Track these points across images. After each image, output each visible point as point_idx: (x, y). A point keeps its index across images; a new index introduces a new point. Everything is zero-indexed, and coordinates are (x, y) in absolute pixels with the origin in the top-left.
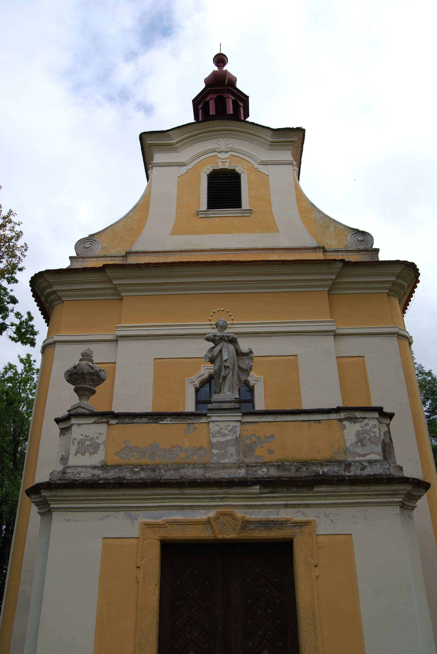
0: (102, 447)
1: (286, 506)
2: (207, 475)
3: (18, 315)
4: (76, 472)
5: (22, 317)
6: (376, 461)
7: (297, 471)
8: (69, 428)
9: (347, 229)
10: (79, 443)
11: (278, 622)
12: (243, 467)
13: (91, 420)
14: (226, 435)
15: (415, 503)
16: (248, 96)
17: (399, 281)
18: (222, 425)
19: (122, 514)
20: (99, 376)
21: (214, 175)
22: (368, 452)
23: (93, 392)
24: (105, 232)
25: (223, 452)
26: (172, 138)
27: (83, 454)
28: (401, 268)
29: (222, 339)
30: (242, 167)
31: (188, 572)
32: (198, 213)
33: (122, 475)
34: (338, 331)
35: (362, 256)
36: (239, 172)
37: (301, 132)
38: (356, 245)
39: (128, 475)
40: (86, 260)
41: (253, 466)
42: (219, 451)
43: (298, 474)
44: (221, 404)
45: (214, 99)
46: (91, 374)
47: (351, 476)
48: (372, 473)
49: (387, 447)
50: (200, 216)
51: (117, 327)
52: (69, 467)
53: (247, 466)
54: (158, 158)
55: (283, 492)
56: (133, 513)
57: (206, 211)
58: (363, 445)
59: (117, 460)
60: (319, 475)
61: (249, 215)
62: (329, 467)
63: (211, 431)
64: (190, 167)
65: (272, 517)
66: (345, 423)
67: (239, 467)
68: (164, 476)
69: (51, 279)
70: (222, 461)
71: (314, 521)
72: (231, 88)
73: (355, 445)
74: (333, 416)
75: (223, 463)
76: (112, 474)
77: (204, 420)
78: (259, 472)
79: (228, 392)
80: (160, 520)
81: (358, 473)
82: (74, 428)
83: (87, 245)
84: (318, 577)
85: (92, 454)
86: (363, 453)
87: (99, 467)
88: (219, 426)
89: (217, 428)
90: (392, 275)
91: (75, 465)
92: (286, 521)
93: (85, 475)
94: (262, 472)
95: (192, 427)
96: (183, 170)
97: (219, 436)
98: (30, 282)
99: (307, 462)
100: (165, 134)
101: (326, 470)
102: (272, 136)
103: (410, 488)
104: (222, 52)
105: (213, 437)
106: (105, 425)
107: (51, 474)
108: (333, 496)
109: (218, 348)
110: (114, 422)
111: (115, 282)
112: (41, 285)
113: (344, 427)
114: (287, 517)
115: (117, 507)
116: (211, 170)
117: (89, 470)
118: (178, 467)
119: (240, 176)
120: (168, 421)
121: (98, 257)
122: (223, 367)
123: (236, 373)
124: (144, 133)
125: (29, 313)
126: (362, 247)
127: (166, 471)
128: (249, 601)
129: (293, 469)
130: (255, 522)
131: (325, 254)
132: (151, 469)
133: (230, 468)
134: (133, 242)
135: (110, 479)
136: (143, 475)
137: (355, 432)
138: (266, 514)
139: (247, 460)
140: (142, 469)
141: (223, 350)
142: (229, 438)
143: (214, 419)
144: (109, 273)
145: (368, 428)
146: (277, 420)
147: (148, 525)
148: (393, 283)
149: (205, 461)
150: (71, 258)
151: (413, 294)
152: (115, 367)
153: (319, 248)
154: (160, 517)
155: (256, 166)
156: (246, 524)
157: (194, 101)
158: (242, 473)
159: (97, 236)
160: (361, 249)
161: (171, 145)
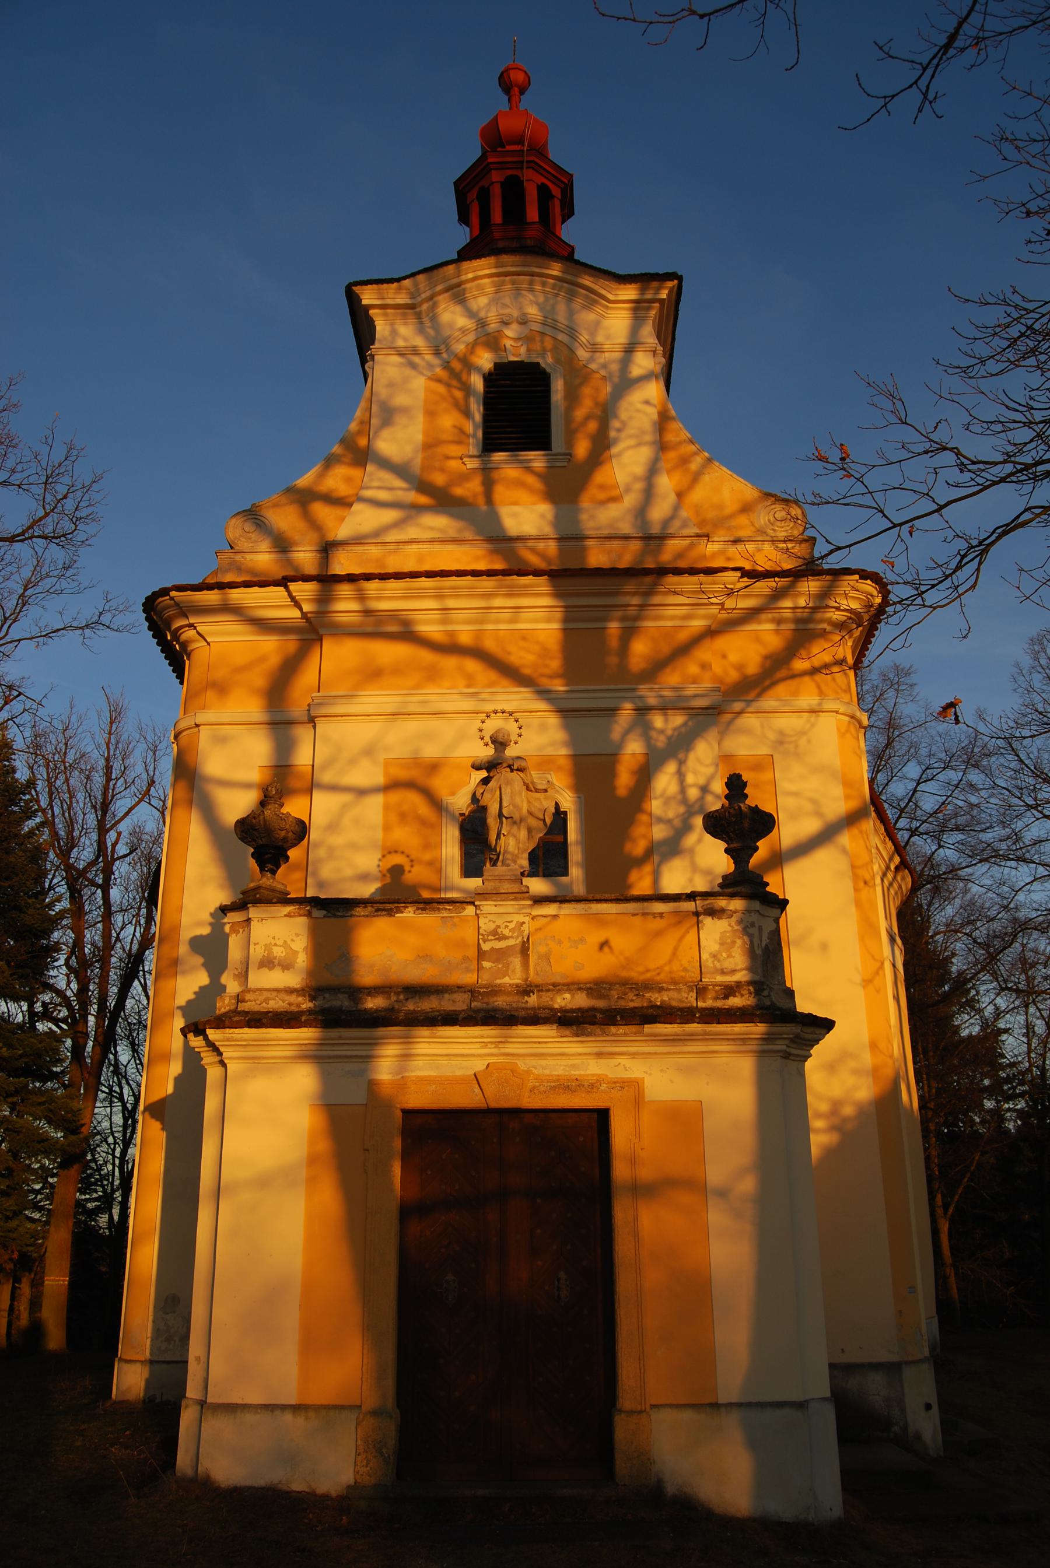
14: (505, 938)
15: (809, 1050)
25: (500, 966)
36: (548, 370)
42: (494, 965)
45: (499, 184)
52: (249, 991)
55: (595, 1035)
63: (481, 931)
65: (577, 1073)
87: (299, 991)
88: (494, 922)
91: (259, 986)
93: (277, 1004)
94: (563, 1001)
97: (495, 939)
98: (143, 605)
112: (166, 611)
117: (283, 995)
119: (549, 378)
137: (719, 935)
138: (568, 1069)
151: (878, 625)
157: (456, 184)
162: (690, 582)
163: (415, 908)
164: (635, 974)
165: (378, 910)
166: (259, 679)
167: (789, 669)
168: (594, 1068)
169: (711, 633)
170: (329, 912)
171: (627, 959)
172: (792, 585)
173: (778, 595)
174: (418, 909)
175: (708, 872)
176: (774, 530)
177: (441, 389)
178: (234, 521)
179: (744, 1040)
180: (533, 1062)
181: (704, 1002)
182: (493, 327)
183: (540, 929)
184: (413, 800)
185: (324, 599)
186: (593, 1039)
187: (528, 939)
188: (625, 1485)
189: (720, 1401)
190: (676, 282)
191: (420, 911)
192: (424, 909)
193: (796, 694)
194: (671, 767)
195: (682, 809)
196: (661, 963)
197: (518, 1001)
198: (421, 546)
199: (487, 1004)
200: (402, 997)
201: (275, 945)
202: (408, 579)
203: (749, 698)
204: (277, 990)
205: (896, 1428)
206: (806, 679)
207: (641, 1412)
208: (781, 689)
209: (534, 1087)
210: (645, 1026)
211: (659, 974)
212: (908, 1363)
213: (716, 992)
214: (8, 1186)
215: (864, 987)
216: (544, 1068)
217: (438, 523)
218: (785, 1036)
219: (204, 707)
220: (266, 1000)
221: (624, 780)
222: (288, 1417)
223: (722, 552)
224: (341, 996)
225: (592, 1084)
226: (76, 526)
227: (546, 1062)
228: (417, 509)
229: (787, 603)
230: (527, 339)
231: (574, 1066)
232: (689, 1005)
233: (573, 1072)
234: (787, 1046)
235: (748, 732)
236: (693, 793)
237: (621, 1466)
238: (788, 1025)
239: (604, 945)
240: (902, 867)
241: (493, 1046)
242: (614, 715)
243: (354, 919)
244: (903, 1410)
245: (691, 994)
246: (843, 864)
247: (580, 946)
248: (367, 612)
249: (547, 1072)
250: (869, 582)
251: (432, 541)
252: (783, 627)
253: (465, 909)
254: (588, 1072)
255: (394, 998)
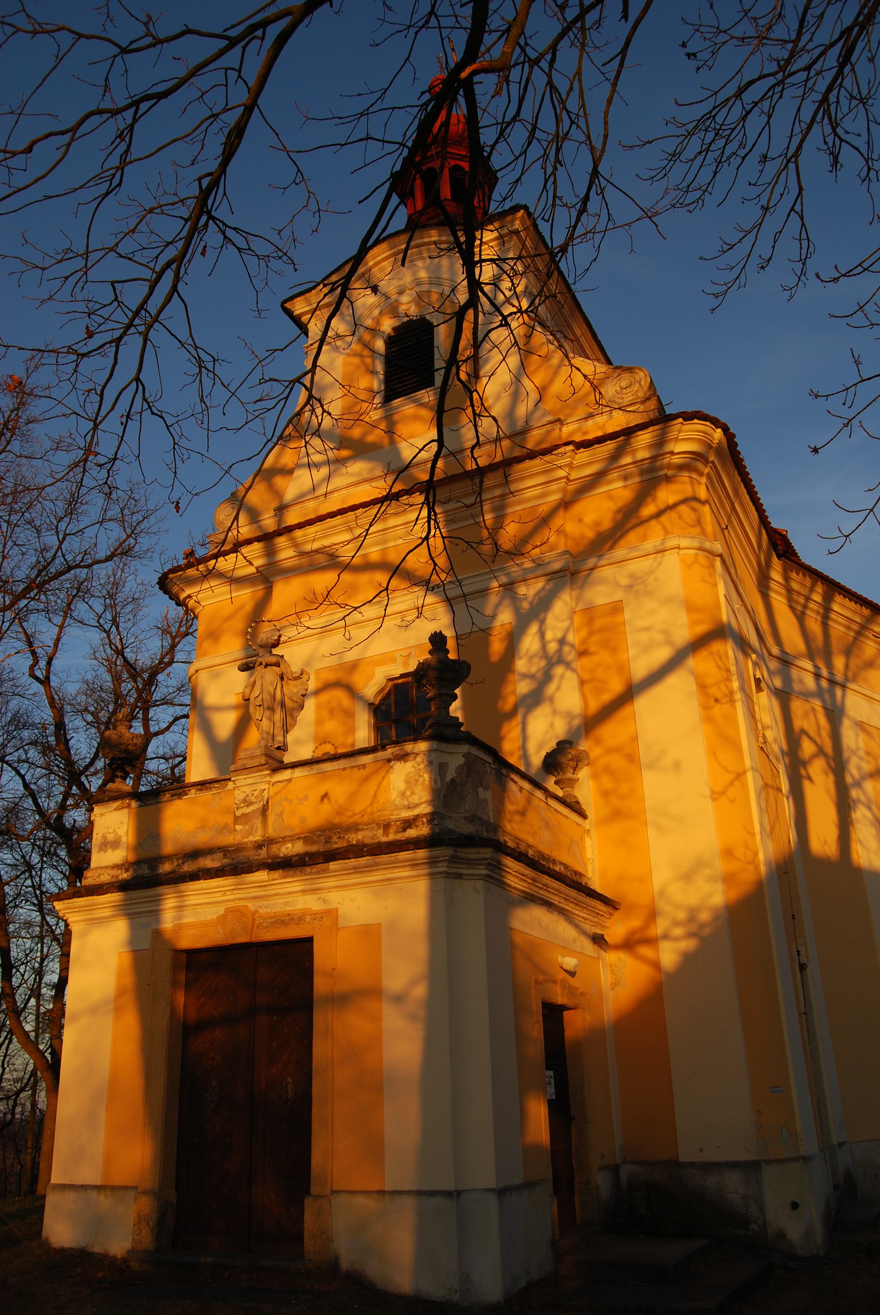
88: (245, 792)
162: (536, 464)
163: (195, 790)
164: (345, 820)
165: (173, 795)
166: (239, 623)
167: (639, 517)
168: (309, 903)
169: (566, 504)
170: (142, 802)
171: (340, 807)
172: (627, 443)
173: (616, 456)
174: (197, 790)
175: (569, 715)
176: (622, 398)
177: (356, 360)
178: (223, 506)
179: (414, 865)
180: (259, 903)
181: (387, 837)
182: (394, 297)
183: (278, 793)
184: (340, 695)
185: (270, 552)
186: (296, 879)
187: (268, 802)
188: (310, 1259)
189: (386, 1189)
190: (522, 211)
191: (199, 792)
192: (201, 790)
193: (644, 538)
194: (534, 628)
195: (543, 663)
196: (363, 806)
197: (254, 855)
198: (340, 493)
199: (233, 859)
200: (180, 861)
201: (109, 833)
202: (318, 523)
203: (600, 553)
204: (106, 867)
205: (754, 1226)
206: (653, 522)
207: (324, 1196)
208: (632, 536)
209: (260, 924)
210: (331, 863)
211: (363, 816)
212: (768, 1162)
213: (397, 826)
215: (714, 800)
216: (267, 907)
217: (358, 468)
218: (442, 859)
219: (205, 654)
220: (99, 876)
221: (497, 646)
222: (94, 1195)
223: (579, 429)
224: (143, 866)
225: (300, 917)
226: (136, 540)
227: (268, 902)
228: (341, 462)
229: (627, 460)
230: (419, 298)
231: (287, 903)
232: (377, 841)
233: (287, 909)
234: (448, 867)
235: (604, 581)
236: (552, 647)
237: (309, 1244)
238: (440, 849)
239: (325, 796)
241: (230, 893)
242: (487, 595)
243: (162, 804)
245: (379, 831)
246: (692, 686)
247: (305, 802)
248: (302, 554)
249: (269, 910)
250: (696, 421)
251: (348, 486)
252: (629, 482)
253: (227, 785)
254: (298, 907)
255: (175, 864)
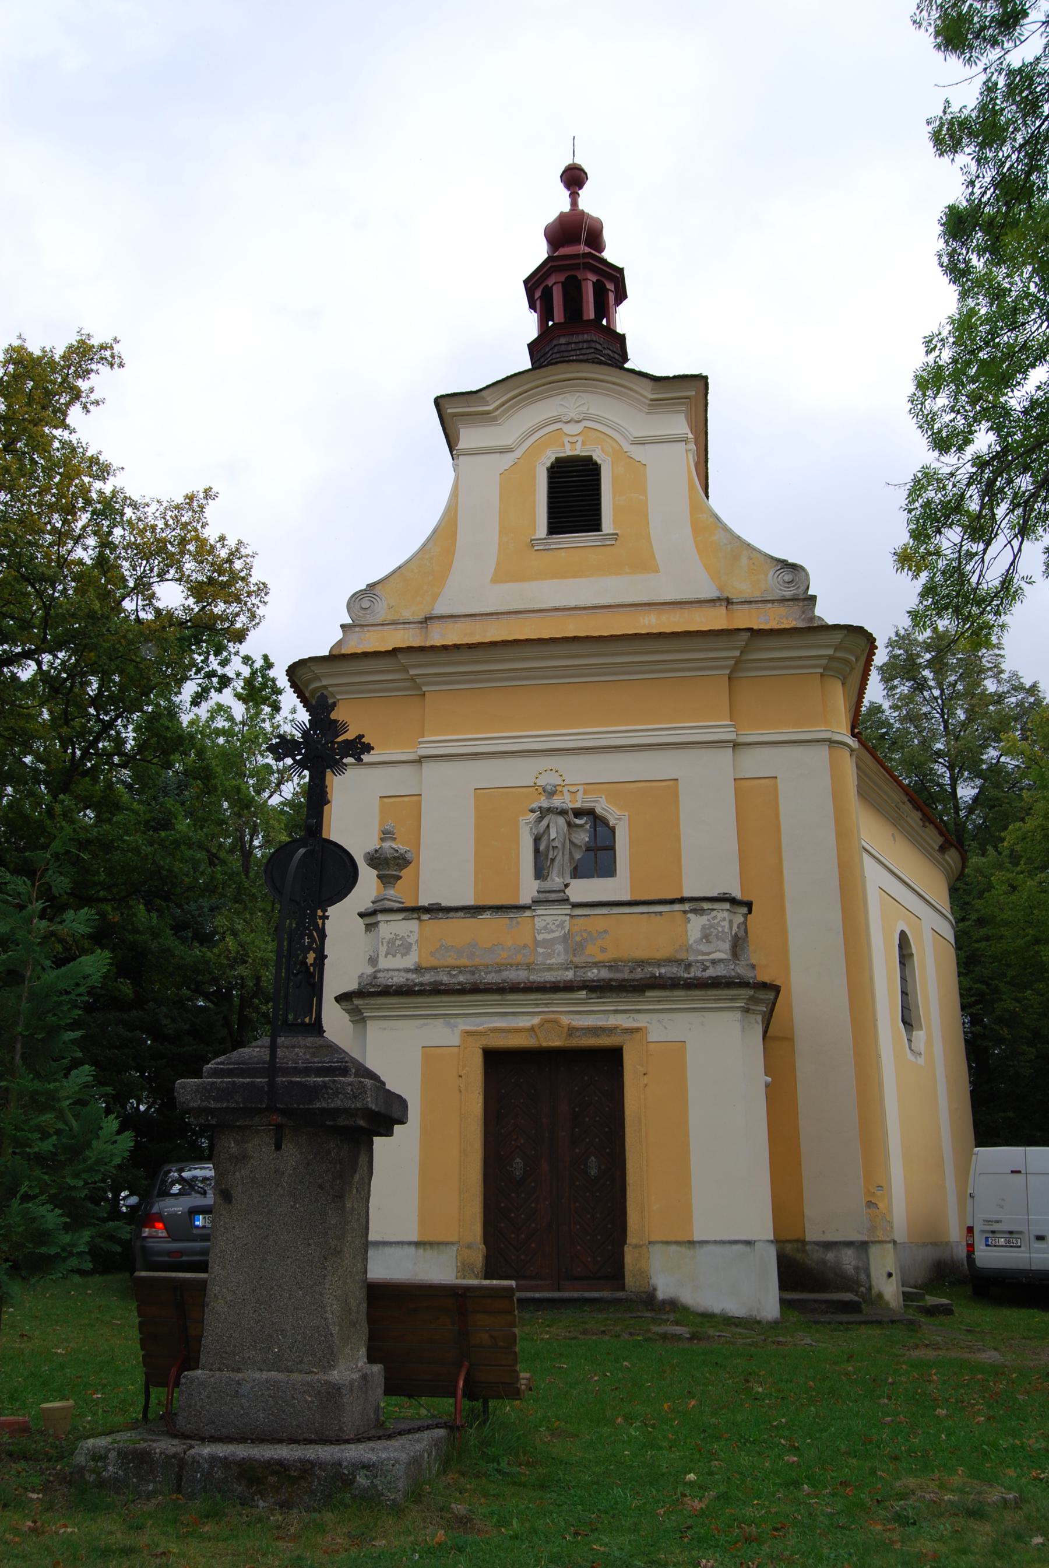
0: (414, 947)
1: (616, 1012)
2: (531, 978)
3: (247, 660)
4: (388, 976)
5: (253, 662)
6: (721, 960)
7: (631, 972)
8: (376, 924)
9: (769, 560)
10: (388, 943)
11: (607, 1130)
12: (571, 968)
13: (401, 916)
14: (553, 931)
16: (621, 266)
17: (839, 654)
18: (549, 919)
19: (439, 1022)
20: (404, 859)
21: (558, 467)
22: (714, 950)
23: (400, 878)
24: (391, 579)
26: (487, 401)
27: (394, 956)
28: (841, 636)
29: (549, 810)
30: (602, 450)
31: (513, 1081)
32: (532, 543)
33: (438, 978)
34: (742, 739)
35: (788, 609)
36: (599, 462)
37: (701, 381)
38: (780, 590)
39: (445, 979)
40: (366, 629)
41: (582, 967)
43: (632, 976)
44: (548, 895)
45: (560, 284)
46: (395, 858)
47: (690, 978)
48: (714, 975)
49: (740, 941)
50: (536, 548)
51: (420, 743)
52: (379, 971)
53: (576, 967)
54: (468, 438)
56: (452, 1021)
57: (545, 539)
58: (708, 941)
59: (432, 962)
60: (656, 977)
61: (613, 542)
62: (667, 968)
63: (536, 927)
64: (518, 453)
66: (690, 915)
67: (567, 969)
68: (484, 979)
69: (318, 670)
70: (548, 962)
71: (646, 1028)
72: (591, 261)
73: (699, 941)
74: (677, 907)
75: (549, 964)
76: (428, 978)
77: (528, 913)
78: (589, 974)
79: (557, 879)
80: (481, 1028)
81: (699, 974)
82: (381, 925)
83: (365, 604)
84: (646, 1085)
85: (403, 955)
86: (708, 951)
89: (543, 924)
90: (828, 646)
91: (386, 968)
92: (616, 1028)
93: (398, 979)
94: (593, 974)
95: (515, 921)
96: (508, 460)
99: (643, 962)
100: (475, 396)
101: (663, 971)
102: (652, 390)
103: (751, 992)
104: (577, 161)
105: (539, 934)
106: (416, 922)
107: (360, 977)
108: (667, 1001)
109: (544, 823)
110: (426, 917)
111: (412, 672)
113: (689, 920)
114: (616, 1023)
115: (435, 1015)
116: (553, 459)
117: (402, 974)
118: (500, 968)
120: (487, 915)
121: (383, 625)
122: (551, 848)
123: (567, 852)
124: (442, 396)
125: (266, 658)
126: (788, 594)
127: (486, 973)
128: (577, 1109)
129: (627, 970)
130: (582, 1029)
131: (730, 607)
132: (470, 971)
133: (558, 969)
134: (436, 596)
135: (426, 984)
136: (461, 978)
139: (576, 960)
140: (460, 972)
141: (551, 825)
142: (557, 934)
143: (539, 912)
144: (403, 659)
145: (716, 921)
146: (611, 912)
147: (469, 1033)
148: (831, 658)
149: (531, 961)
150: (342, 626)
152: (420, 801)
153: (719, 599)
154: (482, 1024)
155: (626, 447)
156: (572, 1031)
157: (526, 282)
158: (569, 975)
159: (379, 587)
160: (788, 597)
161: (488, 413)
214: (938, 553)
237: (629, 1281)
240: (947, 845)
244: (869, 1276)
